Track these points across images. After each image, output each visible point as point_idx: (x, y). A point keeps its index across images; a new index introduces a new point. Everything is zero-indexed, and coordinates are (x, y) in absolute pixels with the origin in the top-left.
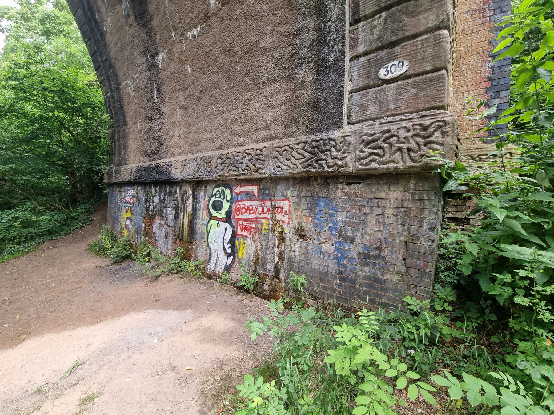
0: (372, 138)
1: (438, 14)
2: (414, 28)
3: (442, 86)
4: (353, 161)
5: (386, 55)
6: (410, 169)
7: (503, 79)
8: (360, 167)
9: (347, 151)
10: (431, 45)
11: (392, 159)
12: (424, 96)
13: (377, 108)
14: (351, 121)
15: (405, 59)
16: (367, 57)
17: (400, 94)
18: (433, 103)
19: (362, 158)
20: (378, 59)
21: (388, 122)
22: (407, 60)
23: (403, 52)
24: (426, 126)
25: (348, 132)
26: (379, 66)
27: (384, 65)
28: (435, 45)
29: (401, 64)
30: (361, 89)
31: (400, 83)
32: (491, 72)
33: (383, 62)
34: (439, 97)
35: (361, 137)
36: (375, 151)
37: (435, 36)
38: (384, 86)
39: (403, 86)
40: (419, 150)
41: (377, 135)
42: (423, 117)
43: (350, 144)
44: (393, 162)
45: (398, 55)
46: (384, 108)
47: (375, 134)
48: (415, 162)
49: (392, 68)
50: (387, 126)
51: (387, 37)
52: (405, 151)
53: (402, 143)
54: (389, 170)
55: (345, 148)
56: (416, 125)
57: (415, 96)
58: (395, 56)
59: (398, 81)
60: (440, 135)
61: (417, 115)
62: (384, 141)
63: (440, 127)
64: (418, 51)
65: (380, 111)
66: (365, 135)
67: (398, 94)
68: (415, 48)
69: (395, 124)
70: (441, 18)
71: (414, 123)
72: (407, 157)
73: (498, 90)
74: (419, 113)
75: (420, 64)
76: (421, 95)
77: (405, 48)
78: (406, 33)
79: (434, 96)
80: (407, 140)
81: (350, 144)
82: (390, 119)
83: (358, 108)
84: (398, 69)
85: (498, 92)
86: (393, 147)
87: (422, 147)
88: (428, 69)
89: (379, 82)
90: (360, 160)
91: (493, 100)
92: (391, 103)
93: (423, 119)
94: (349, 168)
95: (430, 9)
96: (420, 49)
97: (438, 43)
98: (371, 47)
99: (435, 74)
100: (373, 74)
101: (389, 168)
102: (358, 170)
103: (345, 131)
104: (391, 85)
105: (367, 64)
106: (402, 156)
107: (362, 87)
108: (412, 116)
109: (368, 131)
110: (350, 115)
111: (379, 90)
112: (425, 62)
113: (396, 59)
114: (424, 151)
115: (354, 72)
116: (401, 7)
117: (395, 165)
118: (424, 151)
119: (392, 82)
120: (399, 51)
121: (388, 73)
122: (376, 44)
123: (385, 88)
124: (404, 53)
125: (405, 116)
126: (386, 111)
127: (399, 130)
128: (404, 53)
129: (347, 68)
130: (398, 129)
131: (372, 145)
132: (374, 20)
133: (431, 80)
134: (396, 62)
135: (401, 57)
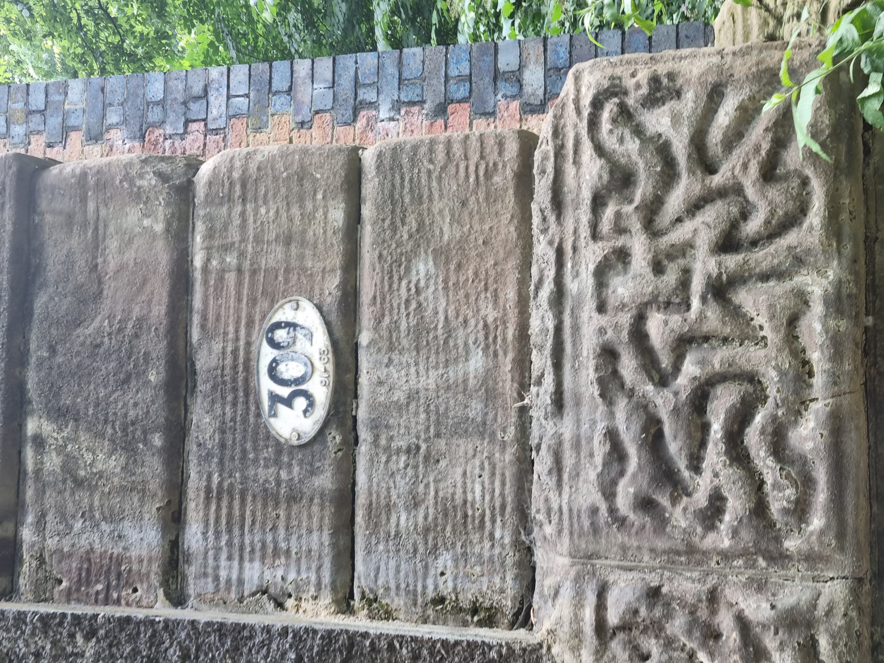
0: (632, 451)
1: (130, 194)
2: (148, 288)
3: (431, 151)
4: (775, 575)
5: (218, 406)
6: (847, 230)
7: (452, 66)
8: (816, 522)
9: (703, 613)
10: (243, 214)
11: (776, 329)
12: (456, 220)
13: (464, 446)
14: (508, 604)
15: (264, 317)
16: (192, 505)
17: (419, 331)
18: (497, 179)
19: (760, 509)
20: (223, 446)
21: (558, 366)
22: (271, 306)
23: (231, 329)
24: (611, 172)
25: (578, 603)
26: (255, 441)
27: (258, 415)
28: (249, 196)
29: (281, 335)
30: (343, 541)
31: (364, 338)
32: (415, 109)
33: (245, 420)
34: (474, 157)
35: (621, 522)
36: (717, 429)
37: (209, 200)
38: (362, 413)
39: (387, 320)
40: (732, 198)
41: (621, 422)
42: (558, 203)
43: (653, 594)
44: (793, 321)
45: (235, 352)
46: (476, 409)
47: (612, 435)
48: (803, 210)
49: (286, 376)
50: (576, 371)
51: (136, 405)
52: (732, 261)
53: (685, 284)
54: (848, 345)
55: (677, 626)
56: (594, 227)
57: (447, 262)
58: (235, 367)
59: (356, 347)
60: (666, 108)
61: (545, 231)
62: (663, 381)
63: (625, 114)
64: (247, 265)
65: (483, 430)
66: (609, 494)
67: (418, 338)
68: (231, 278)
69: (576, 328)
70: (149, 181)
71: (585, 232)
72: (772, 249)
73: (488, 79)
74: (536, 220)
75: (308, 252)
76: (447, 232)
77: (218, 319)
78: (153, 320)
79: (467, 177)
80: (671, 257)
81: (653, 594)
82: (540, 361)
83: (445, 560)
84: (298, 347)
85: (496, 76)
86: (705, 328)
87: (717, 180)
88: (337, 215)
89: (335, 437)
90: (772, 525)
91: (528, 89)
92: (454, 374)
93: (569, 198)
94: (822, 603)
95: (96, 229)
96: (242, 255)
97: (244, 186)
98: (154, 485)
99: (370, 187)
100: (284, 475)
101: (836, 344)
102: (841, 536)
103: (564, 632)
104: (364, 380)
105: (224, 503)
106: (765, 277)
107: (334, 534)
108: (542, 250)
109: (591, 473)
110: (475, 611)
111: (377, 437)
112: (304, 232)
113: (247, 360)
114: (745, 166)
115: (241, 582)
116: (39, 348)
117: (817, 308)
118: (745, 166)
119: (349, 377)
120: (217, 347)
121: (306, 394)
122: (148, 459)
123: (373, 406)
124: (238, 322)
125: (538, 288)
126: (491, 395)
127: (612, 302)
128: (238, 322)
129: (205, 615)
130: (601, 308)
131: (675, 447)
132: (38, 472)
133: (392, 196)
134: (267, 354)
135: (249, 335)
